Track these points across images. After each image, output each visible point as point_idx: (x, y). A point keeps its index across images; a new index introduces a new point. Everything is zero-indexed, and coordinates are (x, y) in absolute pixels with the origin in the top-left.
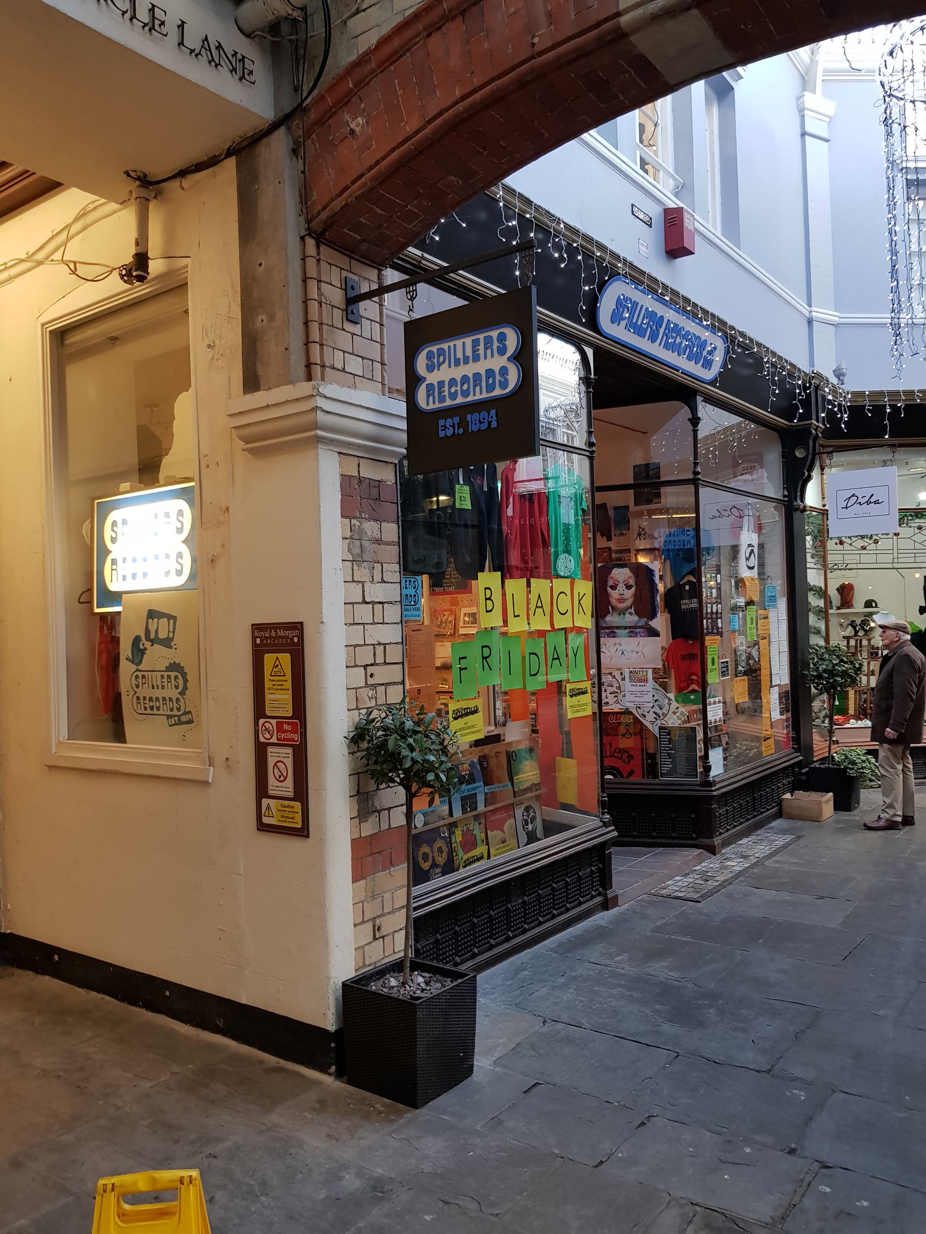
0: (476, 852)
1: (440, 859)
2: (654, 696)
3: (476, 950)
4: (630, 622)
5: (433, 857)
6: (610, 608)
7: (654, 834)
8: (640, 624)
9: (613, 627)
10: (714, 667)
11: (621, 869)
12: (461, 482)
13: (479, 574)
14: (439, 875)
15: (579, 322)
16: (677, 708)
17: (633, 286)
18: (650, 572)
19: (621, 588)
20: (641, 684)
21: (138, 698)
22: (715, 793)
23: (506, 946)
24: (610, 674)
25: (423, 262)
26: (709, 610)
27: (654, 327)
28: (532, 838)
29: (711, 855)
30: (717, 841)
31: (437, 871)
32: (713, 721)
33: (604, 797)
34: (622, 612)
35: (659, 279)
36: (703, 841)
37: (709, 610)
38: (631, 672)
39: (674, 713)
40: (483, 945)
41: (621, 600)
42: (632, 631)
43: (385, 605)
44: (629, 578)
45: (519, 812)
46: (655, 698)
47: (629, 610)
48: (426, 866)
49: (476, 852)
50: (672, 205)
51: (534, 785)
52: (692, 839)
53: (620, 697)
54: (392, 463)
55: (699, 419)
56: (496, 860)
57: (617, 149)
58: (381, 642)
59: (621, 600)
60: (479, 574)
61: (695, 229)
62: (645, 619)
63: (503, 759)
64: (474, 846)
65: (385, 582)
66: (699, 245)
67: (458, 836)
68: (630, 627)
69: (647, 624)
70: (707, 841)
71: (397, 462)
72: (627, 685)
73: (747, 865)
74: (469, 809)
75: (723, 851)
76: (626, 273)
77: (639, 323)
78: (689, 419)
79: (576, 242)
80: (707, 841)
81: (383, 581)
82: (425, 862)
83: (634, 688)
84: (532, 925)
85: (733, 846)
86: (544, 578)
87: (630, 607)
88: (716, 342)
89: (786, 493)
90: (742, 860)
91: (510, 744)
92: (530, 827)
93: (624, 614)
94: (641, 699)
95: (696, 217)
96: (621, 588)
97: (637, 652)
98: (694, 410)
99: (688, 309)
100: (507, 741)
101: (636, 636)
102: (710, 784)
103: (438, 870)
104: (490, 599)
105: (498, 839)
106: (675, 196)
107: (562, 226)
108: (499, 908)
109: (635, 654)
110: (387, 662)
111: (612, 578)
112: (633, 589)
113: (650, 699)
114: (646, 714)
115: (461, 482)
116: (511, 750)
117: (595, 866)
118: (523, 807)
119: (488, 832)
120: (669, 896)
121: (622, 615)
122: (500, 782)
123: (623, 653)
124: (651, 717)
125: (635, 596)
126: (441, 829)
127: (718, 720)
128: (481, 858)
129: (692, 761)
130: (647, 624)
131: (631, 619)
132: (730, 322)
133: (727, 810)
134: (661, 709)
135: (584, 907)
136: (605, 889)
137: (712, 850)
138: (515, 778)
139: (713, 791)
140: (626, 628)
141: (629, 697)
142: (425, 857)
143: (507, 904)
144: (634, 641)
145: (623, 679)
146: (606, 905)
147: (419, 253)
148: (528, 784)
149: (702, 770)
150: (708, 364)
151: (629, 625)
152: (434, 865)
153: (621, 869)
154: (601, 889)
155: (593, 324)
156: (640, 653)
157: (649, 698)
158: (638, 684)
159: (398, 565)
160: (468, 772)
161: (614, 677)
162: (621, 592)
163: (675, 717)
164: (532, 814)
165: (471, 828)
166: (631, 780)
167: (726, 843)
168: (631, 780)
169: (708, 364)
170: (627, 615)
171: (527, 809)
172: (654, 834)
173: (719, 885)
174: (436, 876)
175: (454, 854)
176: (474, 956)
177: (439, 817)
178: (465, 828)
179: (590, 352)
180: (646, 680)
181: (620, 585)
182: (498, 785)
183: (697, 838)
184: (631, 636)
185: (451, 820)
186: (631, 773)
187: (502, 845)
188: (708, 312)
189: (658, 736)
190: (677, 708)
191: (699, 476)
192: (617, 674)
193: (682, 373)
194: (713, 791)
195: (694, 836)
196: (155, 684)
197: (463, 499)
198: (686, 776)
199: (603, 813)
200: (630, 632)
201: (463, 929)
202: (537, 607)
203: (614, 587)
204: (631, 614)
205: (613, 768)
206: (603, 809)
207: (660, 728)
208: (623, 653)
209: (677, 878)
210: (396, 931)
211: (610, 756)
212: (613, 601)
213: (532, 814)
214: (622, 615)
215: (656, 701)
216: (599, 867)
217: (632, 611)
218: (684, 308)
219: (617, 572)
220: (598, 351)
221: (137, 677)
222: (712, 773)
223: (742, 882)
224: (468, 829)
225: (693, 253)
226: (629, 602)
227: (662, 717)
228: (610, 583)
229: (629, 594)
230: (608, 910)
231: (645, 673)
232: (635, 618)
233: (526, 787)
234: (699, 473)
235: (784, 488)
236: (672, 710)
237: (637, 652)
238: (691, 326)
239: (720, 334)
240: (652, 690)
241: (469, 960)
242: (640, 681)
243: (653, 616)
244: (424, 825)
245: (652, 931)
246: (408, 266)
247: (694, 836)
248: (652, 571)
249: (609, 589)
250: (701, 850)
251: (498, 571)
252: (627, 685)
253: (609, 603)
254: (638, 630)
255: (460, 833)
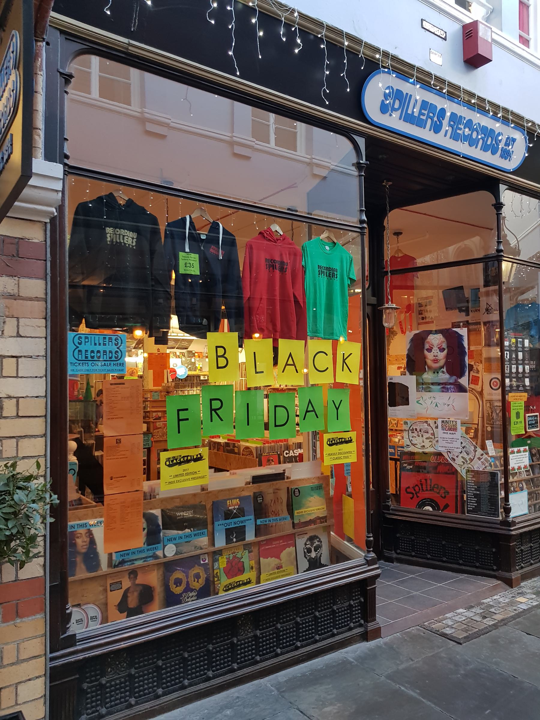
0: (243, 577)
1: (195, 584)
2: (462, 443)
3: (279, 651)
4: (442, 379)
5: (188, 582)
6: (426, 367)
7: (461, 562)
8: (451, 381)
9: (429, 384)
10: (519, 420)
11: (415, 593)
12: (187, 250)
13: (208, 333)
14: (193, 598)
15: (323, 105)
16: (482, 455)
17: (394, 75)
18: (460, 337)
19: (435, 351)
20: (452, 432)
21: (80, 351)
22: (513, 533)
23: (228, 677)
24: (426, 422)
25: (130, 48)
26: (514, 370)
27: (435, 119)
28: (315, 564)
29: (507, 587)
30: (515, 575)
31: (191, 595)
32: (516, 468)
33: (370, 537)
34: (436, 371)
35: (433, 73)
36: (501, 573)
37: (514, 370)
38: (443, 422)
39: (479, 459)
40: (197, 677)
41: (436, 361)
42: (444, 387)
43: (20, 360)
44: (442, 342)
45: (301, 542)
46: (463, 445)
47: (442, 369)
48: (178, 590)
49: (243, 577)
50: (468, 21)
51: (319, 518)
52: (493, 570)
53: (434, 442)
54: (39, 222)
55: (502, 204)
56: (265, 585)
57: (501, 30)
58: (10, 395)
59: (436, 361)
60: (208, 333)
61: (493, 40)
62: (454, 377)
63: (284, 496)
64: (241, 571)
65: (21, 337)
66: (496, 54)
67: (222, 562)
68: (442, 384)
69: (456, 381)
70: (506, 575)
71: (48, 221)
72: (440, 432)
73: (535, 604)
74: (235, 540)
75: (522, 584)
76: (388, 65)
77: (416, 114)
78: (353, 165)
79: (321, 33)
80: (506, 575)
81: (19, 336)
82: (177, 586)
83: (445, 436)
84: (267, 656)
85: (535, 579)
86: (297, 339)
87: (443, 367)
88: (519, 137)
89: (364, 218)
90: (534, 596)
91: (292, 482)
92: (313, 555)
93: (438, 373)
94: (451, 445)
95: (494, 29)
96: (435, 351)
97: (448, 405)
98: (497, 195)
99: (473, 101)
100: (292, 479)
101: (447, 391)
102: (506, 523)
103: (194, 594)
104: (222, 356)
105: (273, 565)
106: (486, 21)
107: (296, 14)
108: (221, 642)
109: (446, 406)
110: (20, 414)
111: (428, 342)
112: (446, 351)
113: (459, 445)
114: (455, 458)
115: (187, 250)
116: (294, 487)
117: (518, 548)
118: (306, 537)
119: (261, 559)
120: (436, 632)
121: (436, 373)
122: (277, 514)
123: (436, 405)
124: (459, 461)
125: (448, 356)
126: (202, 557)
127: (522, 467)
128: (249, 582)
129: (493, 501)
130: (456, 381)
131: (444, 377)
132: (527, 116)
133: (531, 547)
134: (468, 454)
135: (337, 638)
136: (366, 621)
137: (510, 583)
138: (296, 513)
139: (512, 530)
140: (439, 384)
141: (441, 443)
142: (178, 582)
143: (232, 638)
144: (446, 395)
145: (437, 427)
146: (365, 637)
147: (125, 40)
148: (313, 517)
149: (503, 510)
150: (506, 155)
151: (441, 382)
152: (188, 589)
153: (415, 593)
154: (362, 622)
155: (362, 116)
156: (451, 406)
157: (457, 444)
158: (449, 432)
159: (44, 321)
160: (237, 507)
161: (429, 425)
162: (436, 354)
163: (480, 462)
164: (317, 543)
165: (239, 555)
166: (445, 513)
167: (525, 577)
168: (445, 513)
169: (506, 155)
170: (440, 374)
171: (312, 539)
172: (461, 562)
173: (494, 625)
174: (189, 599)
175: (216, 579)
176: (184, 687)
177: (196, 547)
178: (231, 556)
179: (361, 142)
180: (455, 429)
181: (434, 349)
182: (274, 518)
183: (497, 570)
184: (443, 392)
185: (212, 549)
186: (446, 506)
187: (277, 571)
188: (499, 106)
189: (465, 477)
190: (482, 455)
191: (502, 254)
192: (431, 422)
193: (463, 157)
194: (512, 530)
195: (495, 568)
196: (97, 342)
197: (188, 265)
198: (489, 514)
199: (369, 552)
200: (443, 388)
201: (305, 620)
202: (287, 364)
203: (430, 350)
204: (443, 372)
205: (432, 501)
206: (368, 548)
207: (468, 471)
208: (436, 405)
209: (461, 610)
210: (20, 682)
211: (430, 490)
212: (429, 362)
213: (317, 543)
214: (436, 373)
215: (463, 448)
216: (360, 602)
217: (445, 370)
218: (470, 101)
219: (432, 338)
220: (371, 141)
221: (80, 338)
222: (512, 515)
223: (518, 623)
224: (235, 557)
225: (491, 61)
226: (442, 363)
227: (469, 462)
228: (427, 346)
229: (442, 356)
230: (367, 641)
231: (454, 423)
232: (447, 376)
233: (308, 520)
234: (502, 251)
235: (361, 211)
236: (477, 456)
237: (448, 405)
238: (478, 119)
239: (512, 125)
240: (460, 438)
241: (177, 691)
242: (450, 429)
243: (461, 374)
244: (176, 554)
245: (389, 677)
246: (104, 49)
247: (495, 568)
248: (462, 336)
249: (426, 352)
250: (500, 582)
251: (236, 331)
252: (440, 432)
253: (426, 363)
254: (449, 387)
255: (226, 560)
